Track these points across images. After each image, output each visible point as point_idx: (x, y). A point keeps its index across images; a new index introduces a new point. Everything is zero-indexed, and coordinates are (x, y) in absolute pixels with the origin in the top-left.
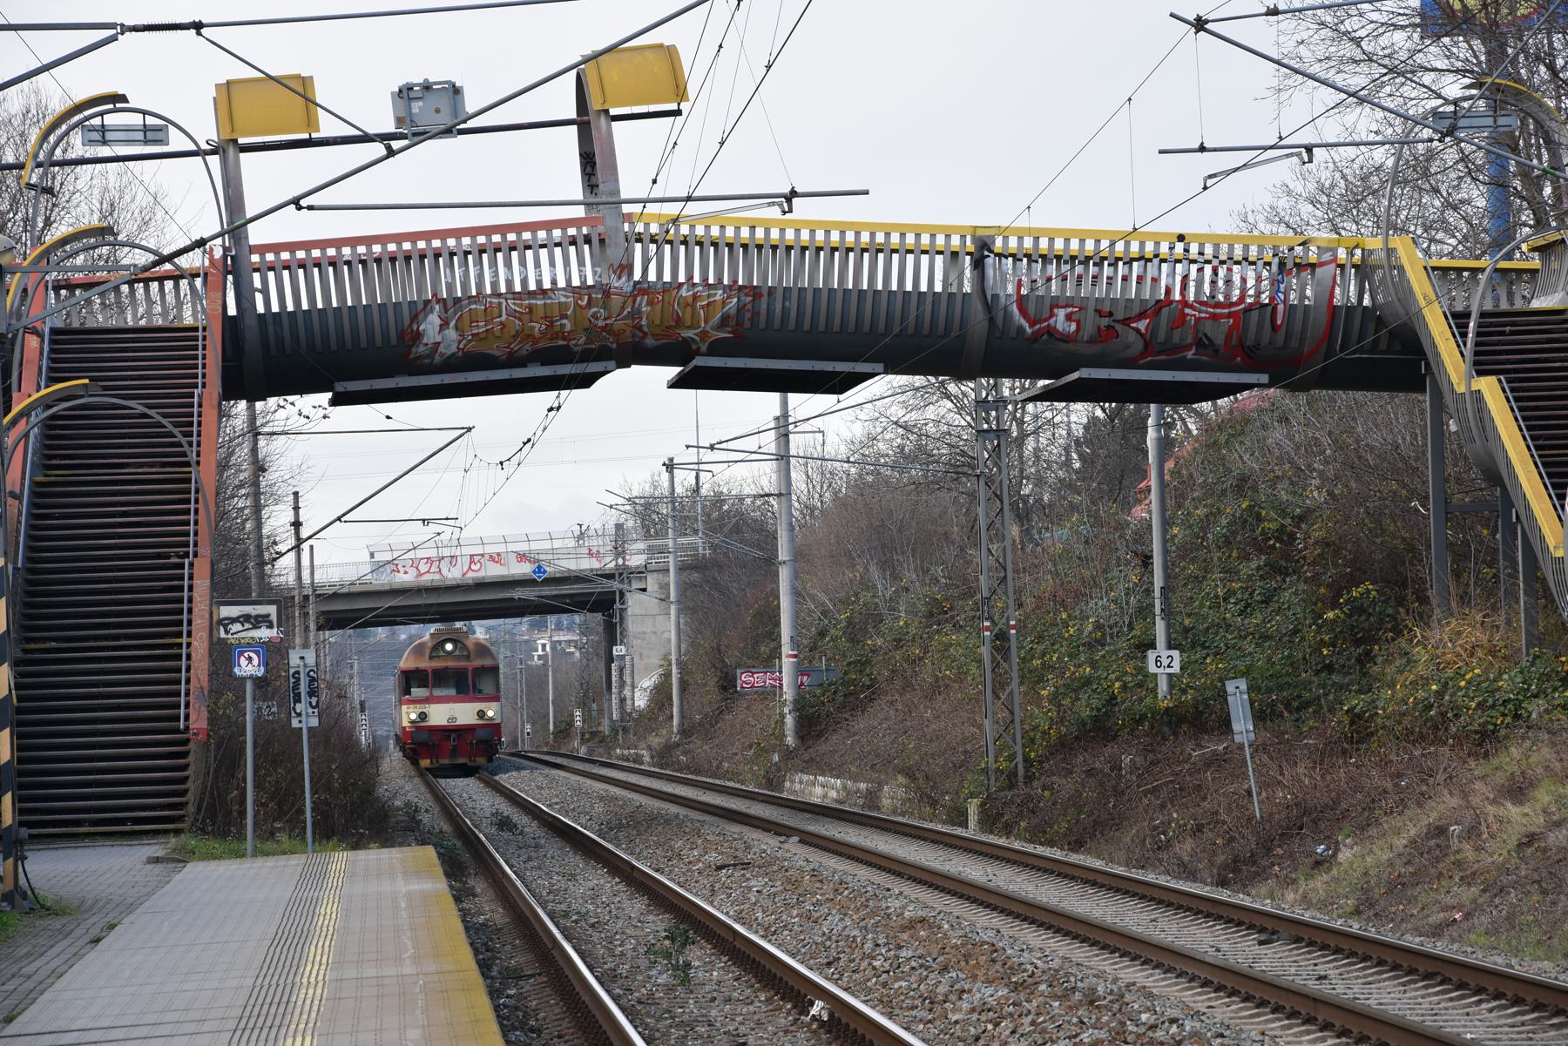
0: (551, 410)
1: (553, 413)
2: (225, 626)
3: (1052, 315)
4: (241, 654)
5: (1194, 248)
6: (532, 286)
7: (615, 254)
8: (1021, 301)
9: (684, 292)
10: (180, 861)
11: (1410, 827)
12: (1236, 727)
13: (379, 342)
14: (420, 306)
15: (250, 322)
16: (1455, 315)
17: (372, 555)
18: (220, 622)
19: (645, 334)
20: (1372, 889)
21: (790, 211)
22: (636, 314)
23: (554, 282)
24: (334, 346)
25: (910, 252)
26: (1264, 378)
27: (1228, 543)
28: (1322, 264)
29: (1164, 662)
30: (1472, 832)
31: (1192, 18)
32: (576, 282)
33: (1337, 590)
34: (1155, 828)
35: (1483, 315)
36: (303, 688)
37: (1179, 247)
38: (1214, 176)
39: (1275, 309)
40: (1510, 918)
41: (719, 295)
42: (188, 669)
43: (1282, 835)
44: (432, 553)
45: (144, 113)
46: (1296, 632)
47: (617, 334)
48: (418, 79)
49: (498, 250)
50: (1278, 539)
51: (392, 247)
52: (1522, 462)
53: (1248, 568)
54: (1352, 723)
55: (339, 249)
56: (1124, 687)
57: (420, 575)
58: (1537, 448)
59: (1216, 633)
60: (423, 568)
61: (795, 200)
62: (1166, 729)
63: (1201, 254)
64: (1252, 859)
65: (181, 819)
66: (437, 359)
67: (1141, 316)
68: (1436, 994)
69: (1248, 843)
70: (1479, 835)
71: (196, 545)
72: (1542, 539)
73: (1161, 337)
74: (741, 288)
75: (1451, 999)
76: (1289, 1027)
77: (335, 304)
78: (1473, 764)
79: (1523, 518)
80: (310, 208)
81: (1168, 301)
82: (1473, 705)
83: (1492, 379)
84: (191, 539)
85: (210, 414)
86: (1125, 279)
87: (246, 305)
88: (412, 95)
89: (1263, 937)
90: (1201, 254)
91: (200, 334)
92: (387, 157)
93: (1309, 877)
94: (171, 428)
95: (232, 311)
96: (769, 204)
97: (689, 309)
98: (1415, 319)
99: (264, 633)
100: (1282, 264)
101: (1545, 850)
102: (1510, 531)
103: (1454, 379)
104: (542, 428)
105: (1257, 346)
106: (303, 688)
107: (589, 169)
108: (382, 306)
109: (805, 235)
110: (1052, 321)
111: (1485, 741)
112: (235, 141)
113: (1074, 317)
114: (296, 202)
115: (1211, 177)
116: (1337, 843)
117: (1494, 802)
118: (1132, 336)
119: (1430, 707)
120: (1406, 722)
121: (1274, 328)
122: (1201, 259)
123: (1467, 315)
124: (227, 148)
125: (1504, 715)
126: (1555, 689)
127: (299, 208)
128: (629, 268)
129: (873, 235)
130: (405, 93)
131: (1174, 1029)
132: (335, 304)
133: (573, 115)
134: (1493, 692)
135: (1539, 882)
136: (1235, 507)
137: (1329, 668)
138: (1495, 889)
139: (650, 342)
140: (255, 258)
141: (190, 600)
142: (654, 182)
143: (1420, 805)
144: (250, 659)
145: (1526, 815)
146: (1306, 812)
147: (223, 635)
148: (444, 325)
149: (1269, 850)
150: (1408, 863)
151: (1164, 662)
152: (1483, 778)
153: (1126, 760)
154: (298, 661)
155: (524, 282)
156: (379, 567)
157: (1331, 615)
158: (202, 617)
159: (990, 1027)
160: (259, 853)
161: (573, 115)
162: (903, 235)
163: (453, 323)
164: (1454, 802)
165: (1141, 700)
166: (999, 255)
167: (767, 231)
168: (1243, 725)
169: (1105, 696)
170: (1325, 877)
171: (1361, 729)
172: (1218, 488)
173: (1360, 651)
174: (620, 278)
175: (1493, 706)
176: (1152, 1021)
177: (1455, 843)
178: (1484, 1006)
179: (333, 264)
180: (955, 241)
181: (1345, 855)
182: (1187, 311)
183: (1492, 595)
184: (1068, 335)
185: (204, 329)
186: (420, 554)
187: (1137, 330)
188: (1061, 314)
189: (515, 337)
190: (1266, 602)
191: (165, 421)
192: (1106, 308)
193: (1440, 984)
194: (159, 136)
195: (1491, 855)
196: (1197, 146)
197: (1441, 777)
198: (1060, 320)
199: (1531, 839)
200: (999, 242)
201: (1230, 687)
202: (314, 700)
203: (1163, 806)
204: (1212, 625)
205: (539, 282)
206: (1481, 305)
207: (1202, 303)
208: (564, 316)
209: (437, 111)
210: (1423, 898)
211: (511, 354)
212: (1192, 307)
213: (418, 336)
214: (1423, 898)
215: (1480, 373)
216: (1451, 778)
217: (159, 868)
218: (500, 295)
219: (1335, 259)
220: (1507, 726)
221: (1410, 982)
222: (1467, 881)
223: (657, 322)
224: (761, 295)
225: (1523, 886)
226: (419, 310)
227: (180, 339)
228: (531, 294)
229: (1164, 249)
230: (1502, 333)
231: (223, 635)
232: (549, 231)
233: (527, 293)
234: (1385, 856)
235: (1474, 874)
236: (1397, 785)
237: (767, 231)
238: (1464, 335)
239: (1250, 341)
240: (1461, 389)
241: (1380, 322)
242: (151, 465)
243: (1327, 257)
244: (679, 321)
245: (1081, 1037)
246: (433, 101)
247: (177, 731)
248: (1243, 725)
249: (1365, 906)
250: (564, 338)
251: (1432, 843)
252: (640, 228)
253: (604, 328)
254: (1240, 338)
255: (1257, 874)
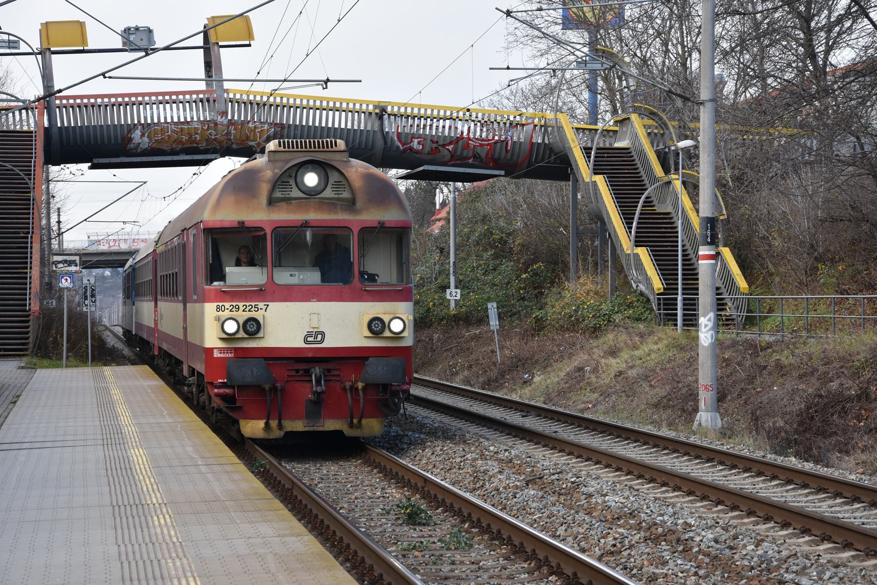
0: (194, 174)
1: (196, 176)
2: (56, 265)
3: (412, 141)
4: (62, 277)
5: (474, 115)
6: (182, 120)
7: (219, 106)
8: (399, 135)
9: (250, 125)
10: (33, 368)
11: (567, 367)
12: (491, 323)
13: (113, 142)
14: (132, 126)
15: (55, 131)
16: (585, 149)
17: (89, 237)
18: (53, 263)
19: (233, 143)
20: (551, 394)
21: (326, 88)
22: (228, 133)
23: (192, 118)
24: (92, 143)
25: (324, 109)
26: (503, 173)
27: (478, 244)
28: (528, 124)
29: (453, 294)
30: (595, 370)
31: (505, 10)
32: (202, 119)
33: (527, 265)
34: (451, 366)
35: (598, 149)
36: (89, 294)
37: (468, 114)
38: (513, 80)
39: (507, 143)
40: (613, 407)
41: (266, 127)
42: (30, 283)
43: (509, 370)
44: (116, 237)
45: (9, 34)
46: (509, 282)
47: (220, 142)
48: (133, 25)
49: (134, 104)
50: (500, 243)
51: (85, 101)
52: (614, 212)
53: (486, 255)
54: (536, 323)
55: (96, 99)
56: (434, 305)
57: (110, 247)
58: (620, 207)
59: (473, 283)
60: (112, 244)
61: (328, 83)
62: (453, 323)
63: (477, 117)
64: (496, 380)
65: (26, 350)
66: (139, 150)
67: (450, 144)
68: (608, 440)
69: (494, 373)
70: (598, 372)
71: (33, 228)
72: (621, 246)
73: (459, 153)
74: (276, 124)
75: (616, 442)
76: (553, 454)
77: (72, 125)
78: (591, 341)
79: (613, 236)
80: (110, 77)
81: (462, 137)
82: (591, 316)
83: (601, 176)
84: (31, 226)
85: (38, 170)
86: (418, 126)
87: (53, 122)
88: (130, 32)
89: (524, 414)
90: (477, 117)
91: (34, 134)
92: (145, 56)
93: (521, 388)
94: (23, 176)
95: (46, 124)
96: (317, 85)
97: (252, 133)
98: (567, 150)
99: (73, 268)
100: (511, 124)
101: (627, 378)
102: (604, 242)
103: (584, 176)
104: (189, 182)
105: (499, 158)
106: (89, 294)
107: (208, 69)
108: (87, 127)
109: (285, 101)
110: (412, 144)
111: (596, 331)
112: (49, 49)
113: (421, 143)
114: (103, 74)
115: (511, 81)
116: (533, 373)
117: (603, 357)
118: (446, 152)
119: (571, 316)
120: (561, 322)
121: (507, 151)
122: (477, 120)
123: (591, 149)
124: (45, 53)
125: (604, 320)
126: (625, 310)
127: (105, 77)
128: (227, 113)
129: (335, 103)
130: (127, 31)
131: (507, 454)
132: (72, 125)
133: (202, 44)
134: (599, 311)
135: (625, 391)
136: (481, 229)
137: (523, 299)
138: (605, 394)
139: (234, 146)
140: (58, 102)
141: (31, 253)
142: (258, 73)
143: (570, 358)
144: (66, 280)
145: (618, 363)
146: (520, 360)
147: (54, 269)
148: (143, 135)
149: (504, 376)
150: (567, 382)
151: (453, 294)
152: (597, 347)
153: (436, 336)
154: (87, 282)
155: (179, 118)
156: (93, 243)
157: (524, 276)
158: (37, 261)
159: (421, 451)
160: (67, 366)
161: (202, 44)
162: (354, 104)
163: (146, 135)
164: (586, 357)
165: (441, 311)
166: (389, 115)
167: (288, 100)
168: (494, 323)
169: (426, 308)
170: (529, 388)
171: (540, 326)
172: (474, 220)
173: (536, 292)
174: (222, 117)
175: (599, 316)
176: (496, 450)
177: (587, 375)
178: (631, 445)
179: (79, 106)
180: (371, 107)
181: (537, 379)
182: (470, 142)
183: (597, 267)
184: (419, 151)
185: (36, 132)
186: (110, 238)
187: (448, 150)
188: (416, 141)
189: (174, 142)
190: (495, 269)
191: (21, 173)
192: (435, 140)
193: (609, 435)
194: (15, 45)
195: (603, 380)
196: (506, 67)
197: (578, 346)
198: (415, 144)
199: (621, 373)
200: (389, 109)
201: (489, 305)
202: (93, 299)
203: (453, 357)
204: (472, 279)
205: (185, 118)
206: (598, 143)
207: (476, 139)
208: (197, 134)
209: (142, 40)
210: (574, 398)
211: (172, 149)
212: (472, 140)
213: (131, 140)
214: (574, 398)
215: (595, 174)
216: (582, 347)
217: (24, 371)
218: (168, 123)
219: (533, 122)
220: (605, 325)
221: (595, 434)
222: (593, 391)
223: (238, 138)
224: (284, 128)
225: (618, 393)
226: (132, 128)
227: (28, 135)
228: (182, 123)
229: (461, 114)
230: (603, 157)
231: (54, 269)
232: (191, 95)
233: (179, 123)
234: (556, 380)
235: (596, 388)
236: (559, 349)
237: (288, 100)
238: (589, 157)
239: (496, 156)
240: (587, 180)
241: (551, 149)
242: (11, 192)
243: (530, 121)
244: (248, 138)
245: (467, 456)
246: (140, 35)
247: (26, 311)
248: (494, 323)
249: (548, 400)
250: (196, 143)
251: (577, 374)
252: (231, 96)
253: (215, 140)
254: (492, 155)
255: (498, 386)
